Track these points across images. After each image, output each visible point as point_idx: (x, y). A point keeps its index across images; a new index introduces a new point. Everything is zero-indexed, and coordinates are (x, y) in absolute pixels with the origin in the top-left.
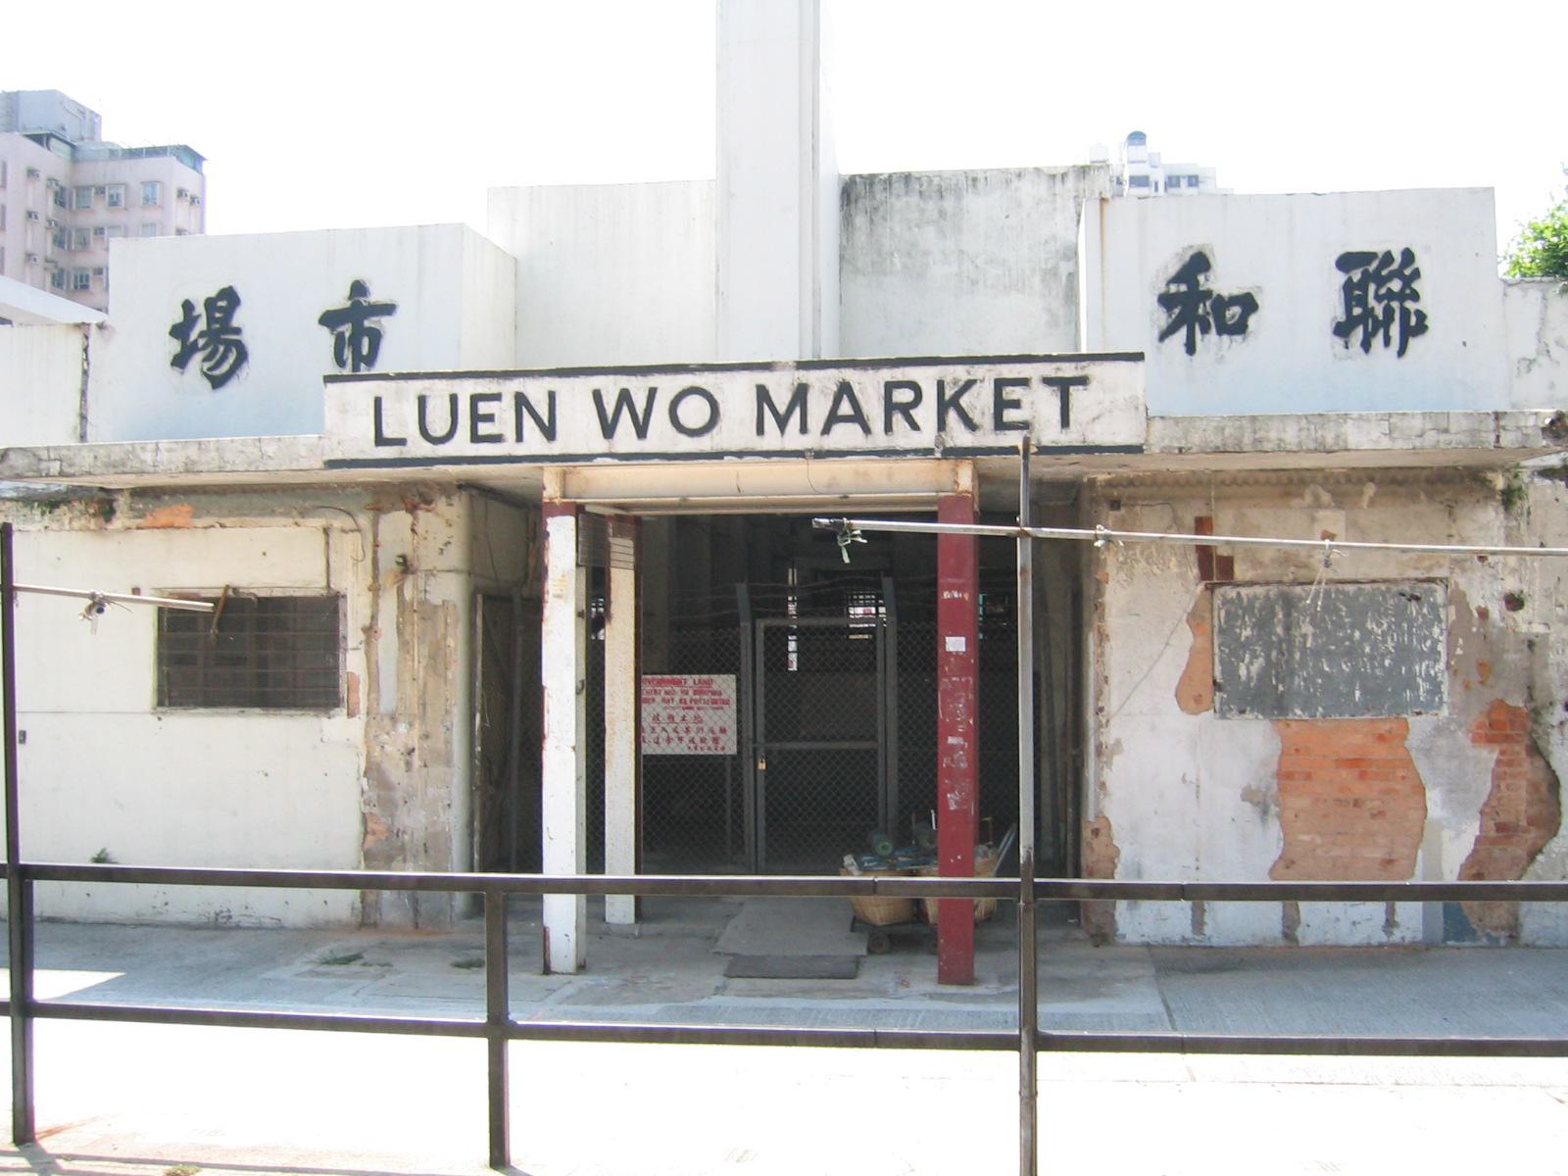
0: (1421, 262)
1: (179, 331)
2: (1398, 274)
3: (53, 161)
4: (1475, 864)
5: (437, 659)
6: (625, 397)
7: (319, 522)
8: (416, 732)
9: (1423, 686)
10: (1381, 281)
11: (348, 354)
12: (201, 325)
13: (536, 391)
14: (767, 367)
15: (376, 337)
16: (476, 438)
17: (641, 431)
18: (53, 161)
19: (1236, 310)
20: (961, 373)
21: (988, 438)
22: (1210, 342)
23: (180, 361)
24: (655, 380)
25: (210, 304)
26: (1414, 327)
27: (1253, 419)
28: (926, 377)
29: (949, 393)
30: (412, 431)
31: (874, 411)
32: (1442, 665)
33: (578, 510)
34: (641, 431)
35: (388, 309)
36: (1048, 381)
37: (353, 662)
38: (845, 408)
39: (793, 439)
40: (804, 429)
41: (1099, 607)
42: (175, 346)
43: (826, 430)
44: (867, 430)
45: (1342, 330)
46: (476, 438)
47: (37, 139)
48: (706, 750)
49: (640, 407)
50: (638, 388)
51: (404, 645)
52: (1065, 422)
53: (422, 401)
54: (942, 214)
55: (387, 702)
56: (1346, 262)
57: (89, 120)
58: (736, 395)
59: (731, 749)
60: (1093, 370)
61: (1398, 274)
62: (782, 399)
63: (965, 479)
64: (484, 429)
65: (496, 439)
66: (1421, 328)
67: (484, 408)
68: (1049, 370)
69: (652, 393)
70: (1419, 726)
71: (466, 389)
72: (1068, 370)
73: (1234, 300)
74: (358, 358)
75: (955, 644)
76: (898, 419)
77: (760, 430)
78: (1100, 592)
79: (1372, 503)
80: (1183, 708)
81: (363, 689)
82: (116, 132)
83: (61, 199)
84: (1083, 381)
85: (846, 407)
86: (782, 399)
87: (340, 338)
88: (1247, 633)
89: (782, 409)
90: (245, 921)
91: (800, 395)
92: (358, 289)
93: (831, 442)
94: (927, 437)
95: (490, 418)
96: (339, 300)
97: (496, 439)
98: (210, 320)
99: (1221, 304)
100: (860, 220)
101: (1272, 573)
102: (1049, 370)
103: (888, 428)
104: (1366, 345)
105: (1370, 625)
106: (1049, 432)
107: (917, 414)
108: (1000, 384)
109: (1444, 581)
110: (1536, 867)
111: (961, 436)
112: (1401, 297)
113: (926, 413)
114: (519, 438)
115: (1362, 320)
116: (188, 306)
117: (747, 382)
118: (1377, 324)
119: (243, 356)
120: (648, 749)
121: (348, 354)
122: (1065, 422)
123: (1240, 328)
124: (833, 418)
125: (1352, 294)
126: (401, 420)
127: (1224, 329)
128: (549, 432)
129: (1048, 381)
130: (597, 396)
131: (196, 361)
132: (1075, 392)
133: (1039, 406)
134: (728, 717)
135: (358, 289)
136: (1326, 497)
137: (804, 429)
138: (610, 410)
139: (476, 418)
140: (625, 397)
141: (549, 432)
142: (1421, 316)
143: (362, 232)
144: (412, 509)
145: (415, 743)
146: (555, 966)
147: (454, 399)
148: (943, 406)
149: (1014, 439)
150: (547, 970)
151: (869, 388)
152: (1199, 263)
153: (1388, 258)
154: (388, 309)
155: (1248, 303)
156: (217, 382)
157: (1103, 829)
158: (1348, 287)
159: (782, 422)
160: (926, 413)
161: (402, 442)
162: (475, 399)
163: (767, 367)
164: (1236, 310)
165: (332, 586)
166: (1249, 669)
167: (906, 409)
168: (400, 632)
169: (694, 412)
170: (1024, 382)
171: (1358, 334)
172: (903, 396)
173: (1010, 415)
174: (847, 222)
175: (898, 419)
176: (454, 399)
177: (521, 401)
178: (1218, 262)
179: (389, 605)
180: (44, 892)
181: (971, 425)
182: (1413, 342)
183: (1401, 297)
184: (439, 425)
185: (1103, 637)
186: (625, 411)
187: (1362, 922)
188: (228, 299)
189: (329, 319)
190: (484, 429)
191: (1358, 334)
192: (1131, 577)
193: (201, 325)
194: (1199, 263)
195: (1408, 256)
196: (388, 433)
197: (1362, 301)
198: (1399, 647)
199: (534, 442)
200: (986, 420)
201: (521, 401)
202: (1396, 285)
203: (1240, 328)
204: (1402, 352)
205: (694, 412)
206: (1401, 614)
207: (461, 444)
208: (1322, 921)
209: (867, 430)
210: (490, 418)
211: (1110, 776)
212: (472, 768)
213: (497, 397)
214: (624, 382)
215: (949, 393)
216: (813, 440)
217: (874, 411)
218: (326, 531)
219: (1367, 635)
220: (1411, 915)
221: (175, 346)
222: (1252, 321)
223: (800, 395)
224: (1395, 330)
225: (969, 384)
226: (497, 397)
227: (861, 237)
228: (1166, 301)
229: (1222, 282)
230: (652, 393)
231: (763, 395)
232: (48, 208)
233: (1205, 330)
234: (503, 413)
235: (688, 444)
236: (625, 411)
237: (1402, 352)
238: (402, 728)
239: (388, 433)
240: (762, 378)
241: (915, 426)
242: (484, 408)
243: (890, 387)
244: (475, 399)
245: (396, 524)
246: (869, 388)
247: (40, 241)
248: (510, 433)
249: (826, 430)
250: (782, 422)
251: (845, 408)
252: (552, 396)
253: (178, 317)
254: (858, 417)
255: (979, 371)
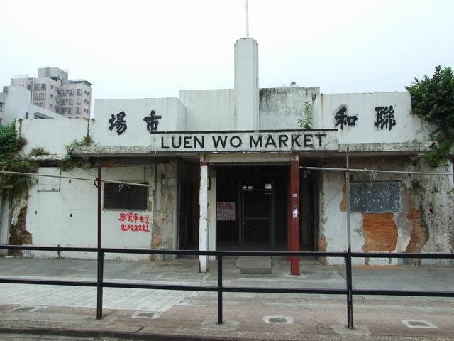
0: (394, 109)
1: (111, 121)
2: (389, 111)
3: (57, 84)
4: (409, 247)
5: (170, 198)
6: (220, 138)
7: (142, 166)
8: (165, 215)
9: (396, 205)
10: (385, 113)
11: (150, 127)
12: (116, 120)
13: (200, 137)
14: (253, 131)
15: (157, 124)
16: (185, 147)
17: (224, 146)
18: (57, 84)
19: (352, 120)
20: (297, 133)
21: (303, 148)
22: (346, 127)
23: (111, 128)
24: (227, 134)
25: (118, 115)
26: (393, 124)
27: (363, 144)
28: (289, 134)
29: (294, 138)
30: (170, 145)
31: (277, 142)
32: (400, 201)
33: (208, 164)
34: (224, 146)
35: (160, 117)
36: (316, 135)
37: (151, 199)
38: (270, 141)
39: (258, 148)
40: (261, 146)
41: (322, 187)
42: (110, 125)
43: (266, 146)
44: (275, 146)
45: (377, 124)
46: (185, 147)
47: (53, 78)
48: (228, 219)
49: (223, 141)
50: (223, 136)
51: (163, 195)
52: (320, 145)
53: (173, 138)
54: (282, 98)
55: (158, 208)
56: (377, 109)
57: (65, 74)
58: (245, 138)
59: (234, 219)
60: (327, 133)
61: (389, 111)
62: (256, 139)
63: (297, 158)
64: (187, 145)
65: (190, 147)
66: (394, 124)
67: (187, 140)
68: (316, 133)
69: (226, 137)
70: (396, 215)
71: (183, 136)
72: (321, 133)
73: (352, 117)
74: (152, 128)
75: (295, 195)
76: (282, 144)
77: (251, 146)
78: (322, 184)
79: (384, 163)
80: (342, 210)
81: (153, 204)
82: (71, 77)
83: (58, 92)
84: (325, 135)
85: (270, 141)
86: (256, 139)
87: (148, 123)
88: (355, 193)
89: (256, 141)
90: (124, 260)
91: (260, 138)
92: (153, 112)
93: (267, 149)
94: (289, 148)
95: (188, 142)
96: (148, 115)
97: (190, 147)
98: (118, 119)
99: (349, 118)
100: (264, 99)
101: (361, 179)
102: (316, 133)
103: (280, 146)
104: (382, 128)
105: (384, 191)
106: (317, 147)
107: (287, 143)
108: (306, 136)
109: (401, 181)
110: (424, 248)
111: (297, 148)
112: (390, 117)
113: (289, 143)
114: (195, 147)
115: (381, 122)
116: (113, 116)
117: (211, 135)
118: (385, 123)
119: (126, 127)
120: (218, 219)
121: (150, 127)
122: (320, 145)
123: (353, 124)
124: (268, 144)
125: (379, 116)
126: (168, 142)
127: (350, 124)
128: (202, 146)
129: (316, 135)
130: (213, 137)
131: (115, 129)
132: (323, 138)
133: (315, 141)
134: (233, 212)
135: (153, 112)
136: (373, 162)
137: (261, 146)
138: (216, 141)
139: (185, 142)
140: (220, 138)
141: (202, 146)
142: (394, 121)
143: (154, 99)
144: (165, 163)
145: (165, 217)
146: (202, 270)
147: (180, 138)
148: (293, 141)
149: (308, 149)
150: (200, 272)
151: (276, 136)
152: (344, 109)
153: (387, 108)
154: (160, 117)
155: (355, 118)
156: (120, 133)
157: (323, 238)
158: (378, 114)
159: (256, 144)
160: (289, 143)
161: (168, 148)
162: (185, 138)
163: (253, 131)
164: (352, 120)
165: (43, 171)
166: (356, 202)
167: (284, 142)
168: (162, 192)
169: (236, 142)
170: (311, 136)
171: (380, 125)
172: (284, 138)
173: (308, 143)
174: (261, 99)
175: (282, 144)
176: (180, 138)
177: (196, 138)
178: (348, 108)
179: (159, 185)
180: (107, 256)
181: (299, 145)
182: (392, 127)
183: (390, 117)
184: (177, 145)
185: (323, 194)
186: (220, 141)
187: (384, 262)
188: (122, 114)
189: (146, 119)
190: (187, 145)
191: (380, 125)
192: (329, 179)
193: (116, 120)
194: (344, 109)
195: (391, 107)
196: (165, 145)
197: (381, 118)
198: (391, 196)
199: (199, 148)
200: (303, 145)
201: (196, 138)
202: (388, 114)
203: (353, 124)
204: (390, 129)
205: (236, 142)
206: (391, 189)
207: (182, 149)
208: (373, 261)
209: (275, 146)
210: (188, 142)
211: (325, 226)
212: (177, 223)
213: (190, 138)
214: (220, 135)
215: (294, 138)
216: (263, 149)
217: (277, 142)
218: (145, 168)
219: (383, 194)
220: (395, 261)
221: (110, 125)
222: (356, 122)
223: (260, 138)
224: (388, 124)
225: (299, 136)
226: (190, 138)
227: (264, 103)
228: (336, 117)
229: (349, 113)
230: (226, 137)
231: (252, 138)
232: (55, 94)
233: (345, 124)
234: (192, 141)
235: (234, 149)
236: (220, 141)
237: (390, 129)
238: (162, 214)
239: (165, 145)
240: (252, 134)
241: (286, 146)
242: (187, 140)
243: (281, 136)
244: (185, 138)
245: (161, 166)
246: (276, 136)
247: (54, 103)
248: (193, 146)
249: (266, 146)
250: (256, 144)
251: (270, 141)
252: (203, 137)
253: (111, 118)
254: (273, 143)
255: (301, 133)
